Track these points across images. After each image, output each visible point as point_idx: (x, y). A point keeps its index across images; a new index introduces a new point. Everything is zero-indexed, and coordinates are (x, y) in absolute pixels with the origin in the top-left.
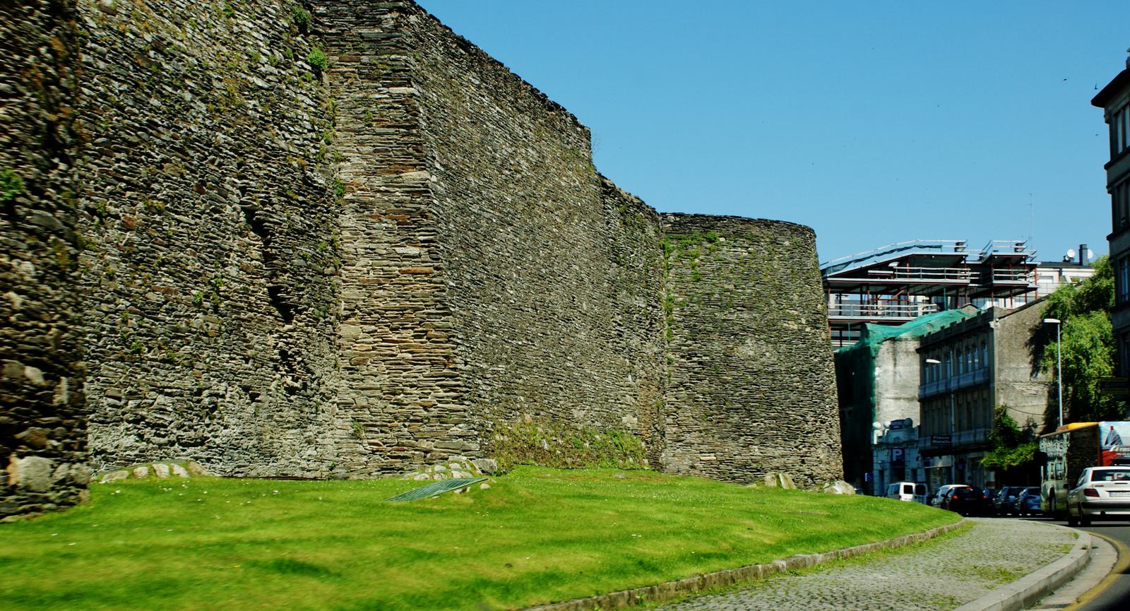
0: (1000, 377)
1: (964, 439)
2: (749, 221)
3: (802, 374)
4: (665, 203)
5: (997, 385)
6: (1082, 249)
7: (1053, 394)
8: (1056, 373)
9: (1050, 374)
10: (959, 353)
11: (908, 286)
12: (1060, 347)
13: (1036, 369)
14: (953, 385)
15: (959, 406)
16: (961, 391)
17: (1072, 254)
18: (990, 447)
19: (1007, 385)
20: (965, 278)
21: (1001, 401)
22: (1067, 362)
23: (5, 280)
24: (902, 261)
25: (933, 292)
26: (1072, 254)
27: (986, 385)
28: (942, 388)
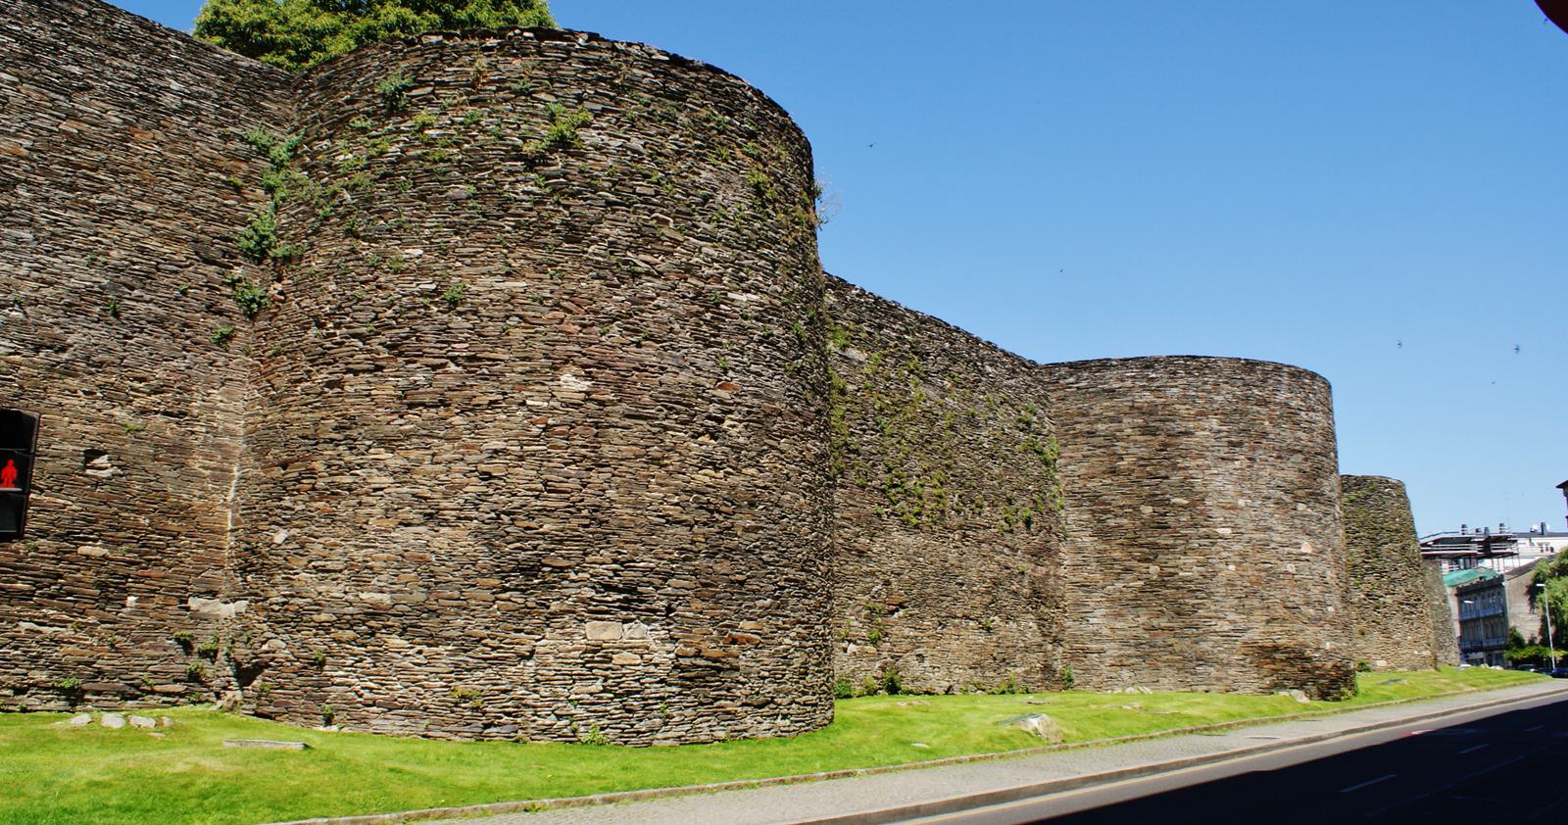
0: (1510, 612)
1: (1491, 644)
2: (1104, 364)
3: (1442, 622)
4: (1042, 361)
5: (1509, 615)
6: (1543, 526)
7: (1544, 620)
8: (1544, 609)
9: (1541, 610)
10: (1483, 598)
11: (1440, 556)
12: (1545, 596)
13: (1532, 607)
14: (1482, 615)
15: (1486, 625)
16: (1486, 618)
17: (1537, 527)
18: (1507, 647)
19: (1514, 615)
20: (1474, 549)
21: (1512, 624)
22: (1550, 604)
23: (8, 209)
24: (1435, 542)
25: (1454, 559)
26: (1537, 527)
27: (1502, 617)
28: (1474, 616)
